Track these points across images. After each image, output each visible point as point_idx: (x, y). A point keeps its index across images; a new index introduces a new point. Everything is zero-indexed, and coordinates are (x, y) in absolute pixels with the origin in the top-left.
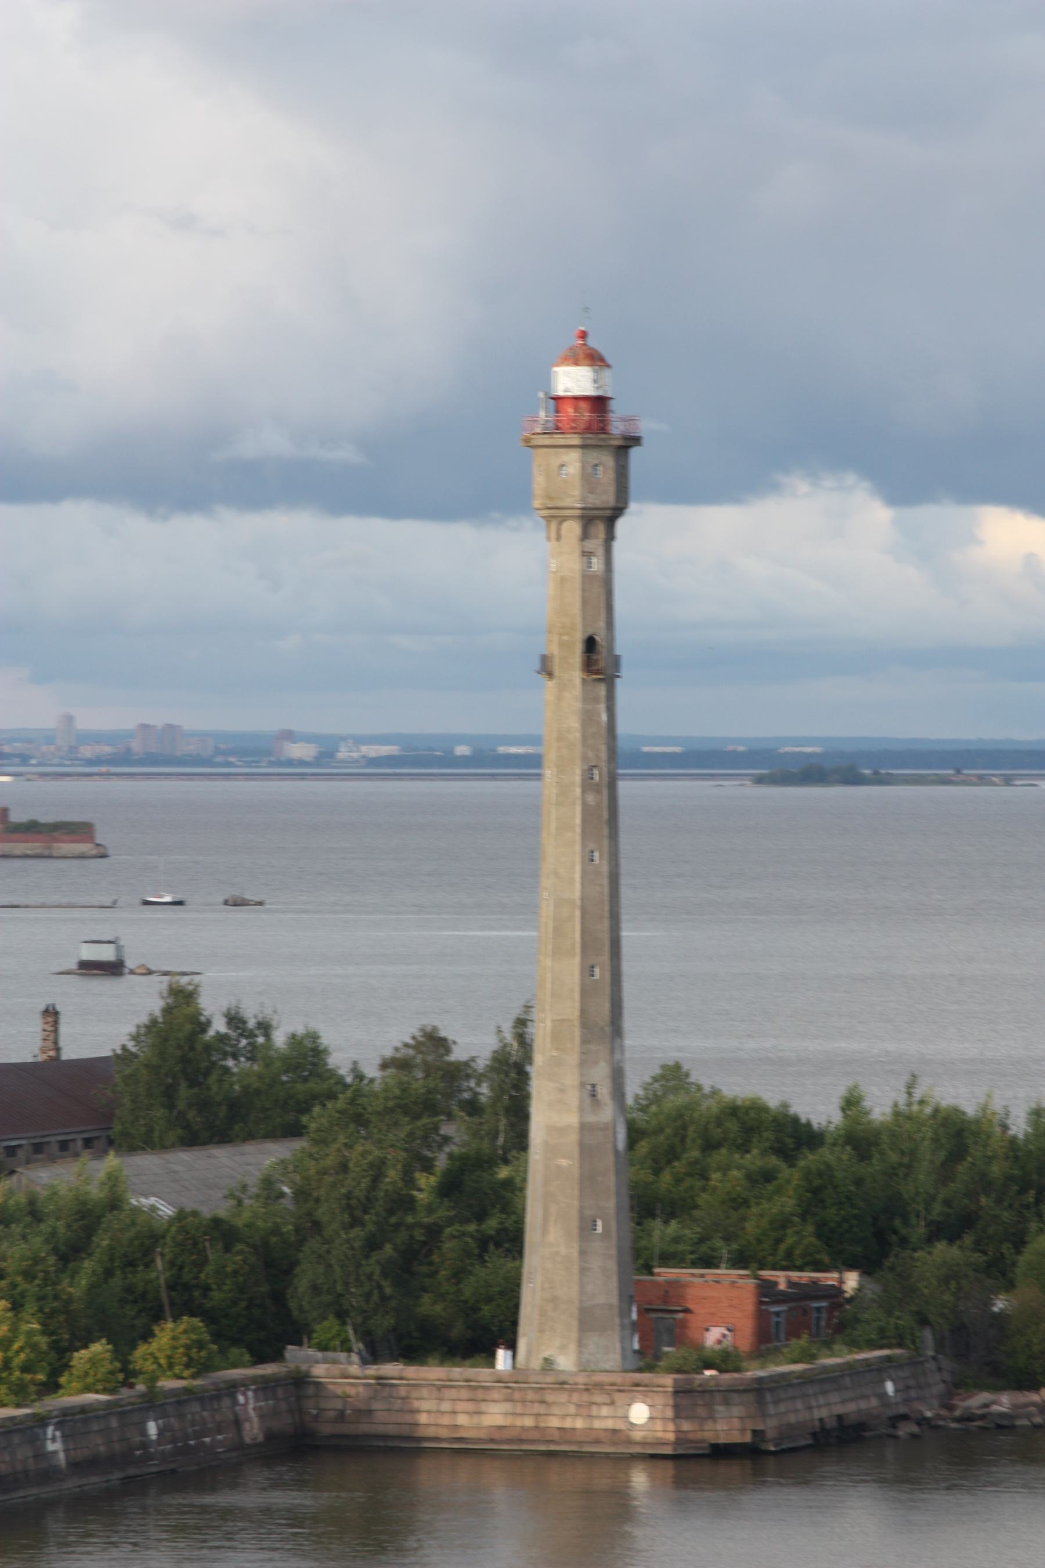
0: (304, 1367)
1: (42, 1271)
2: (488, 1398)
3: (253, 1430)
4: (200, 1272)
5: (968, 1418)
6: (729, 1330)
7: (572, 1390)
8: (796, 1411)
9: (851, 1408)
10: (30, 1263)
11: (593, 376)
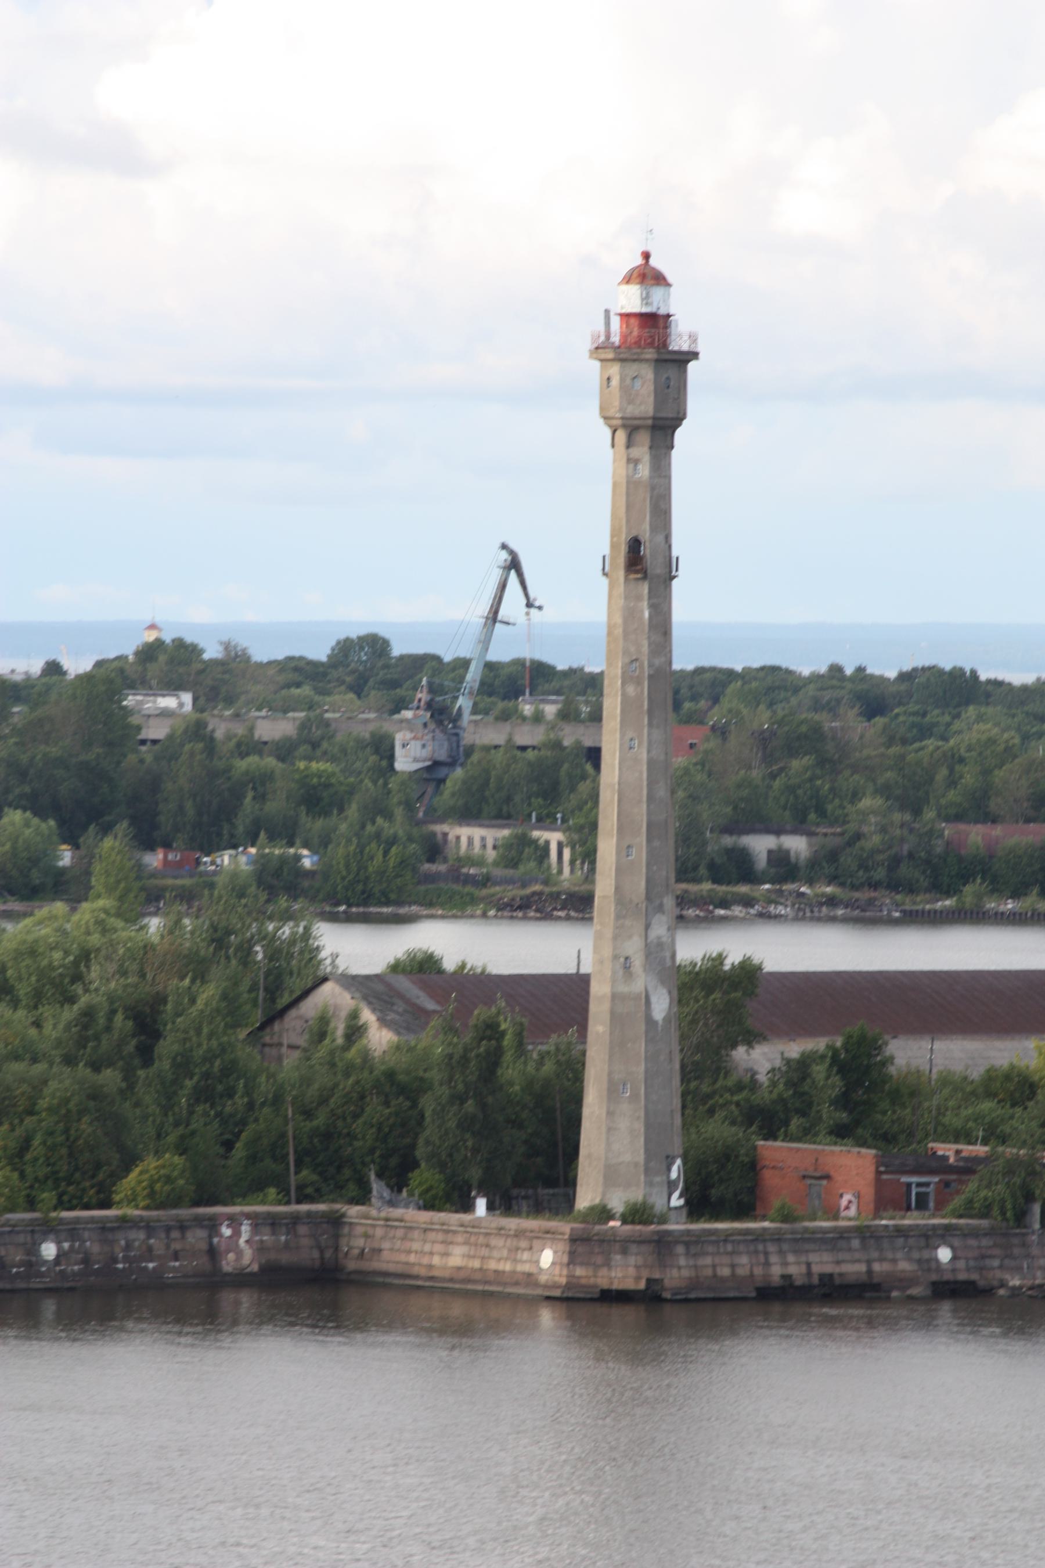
7: (508, 1236)
11: (639, 292)
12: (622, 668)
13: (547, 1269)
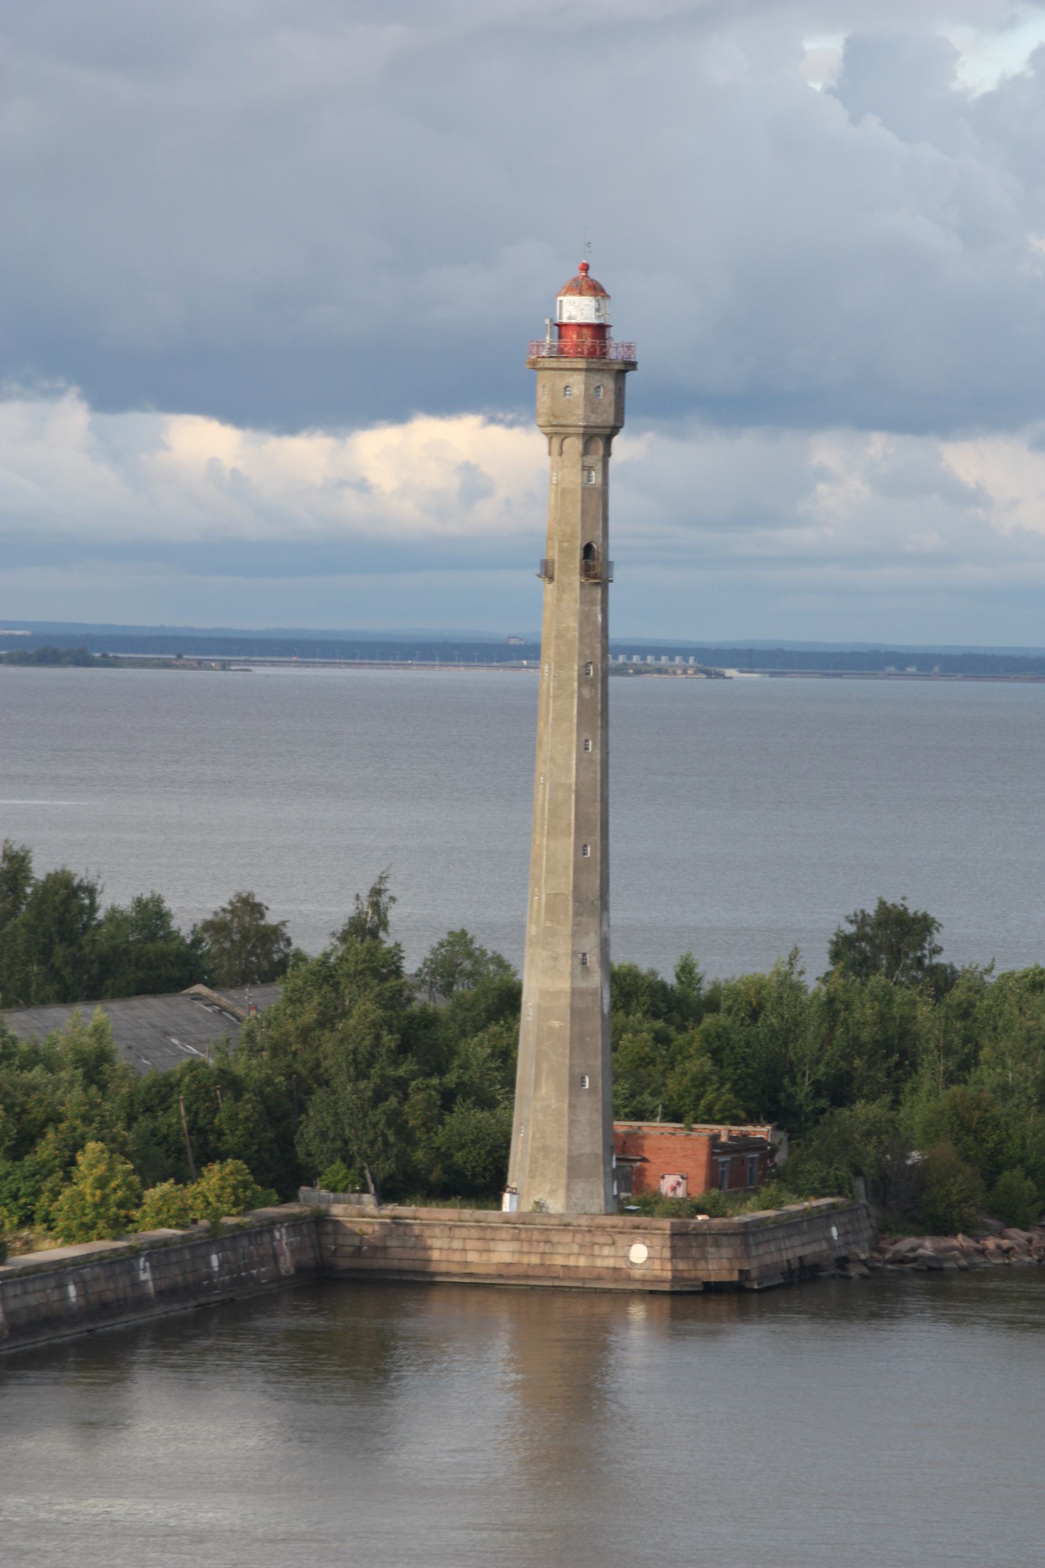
0: (323, 1207)
1: (98, 1115)
2: (497, 1237)
3: (287, 1263)
4: (214, 1118)
5: (900, 1260)
6: (683, 1178)
7: (575, 1232)
8: (771, 1253)
9: (808, 1250)
10: (87, 1107)
12: (578, 671)
13: (642, 1264)
